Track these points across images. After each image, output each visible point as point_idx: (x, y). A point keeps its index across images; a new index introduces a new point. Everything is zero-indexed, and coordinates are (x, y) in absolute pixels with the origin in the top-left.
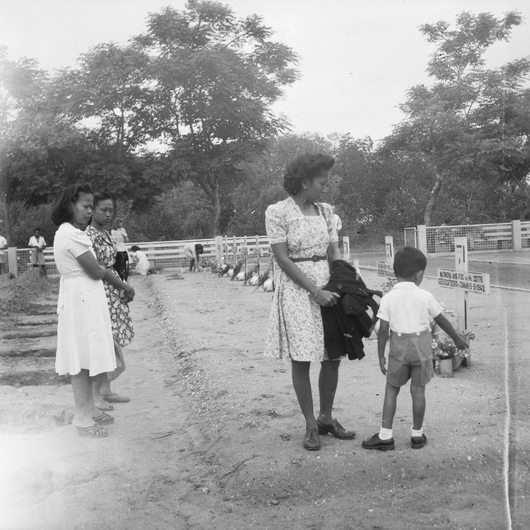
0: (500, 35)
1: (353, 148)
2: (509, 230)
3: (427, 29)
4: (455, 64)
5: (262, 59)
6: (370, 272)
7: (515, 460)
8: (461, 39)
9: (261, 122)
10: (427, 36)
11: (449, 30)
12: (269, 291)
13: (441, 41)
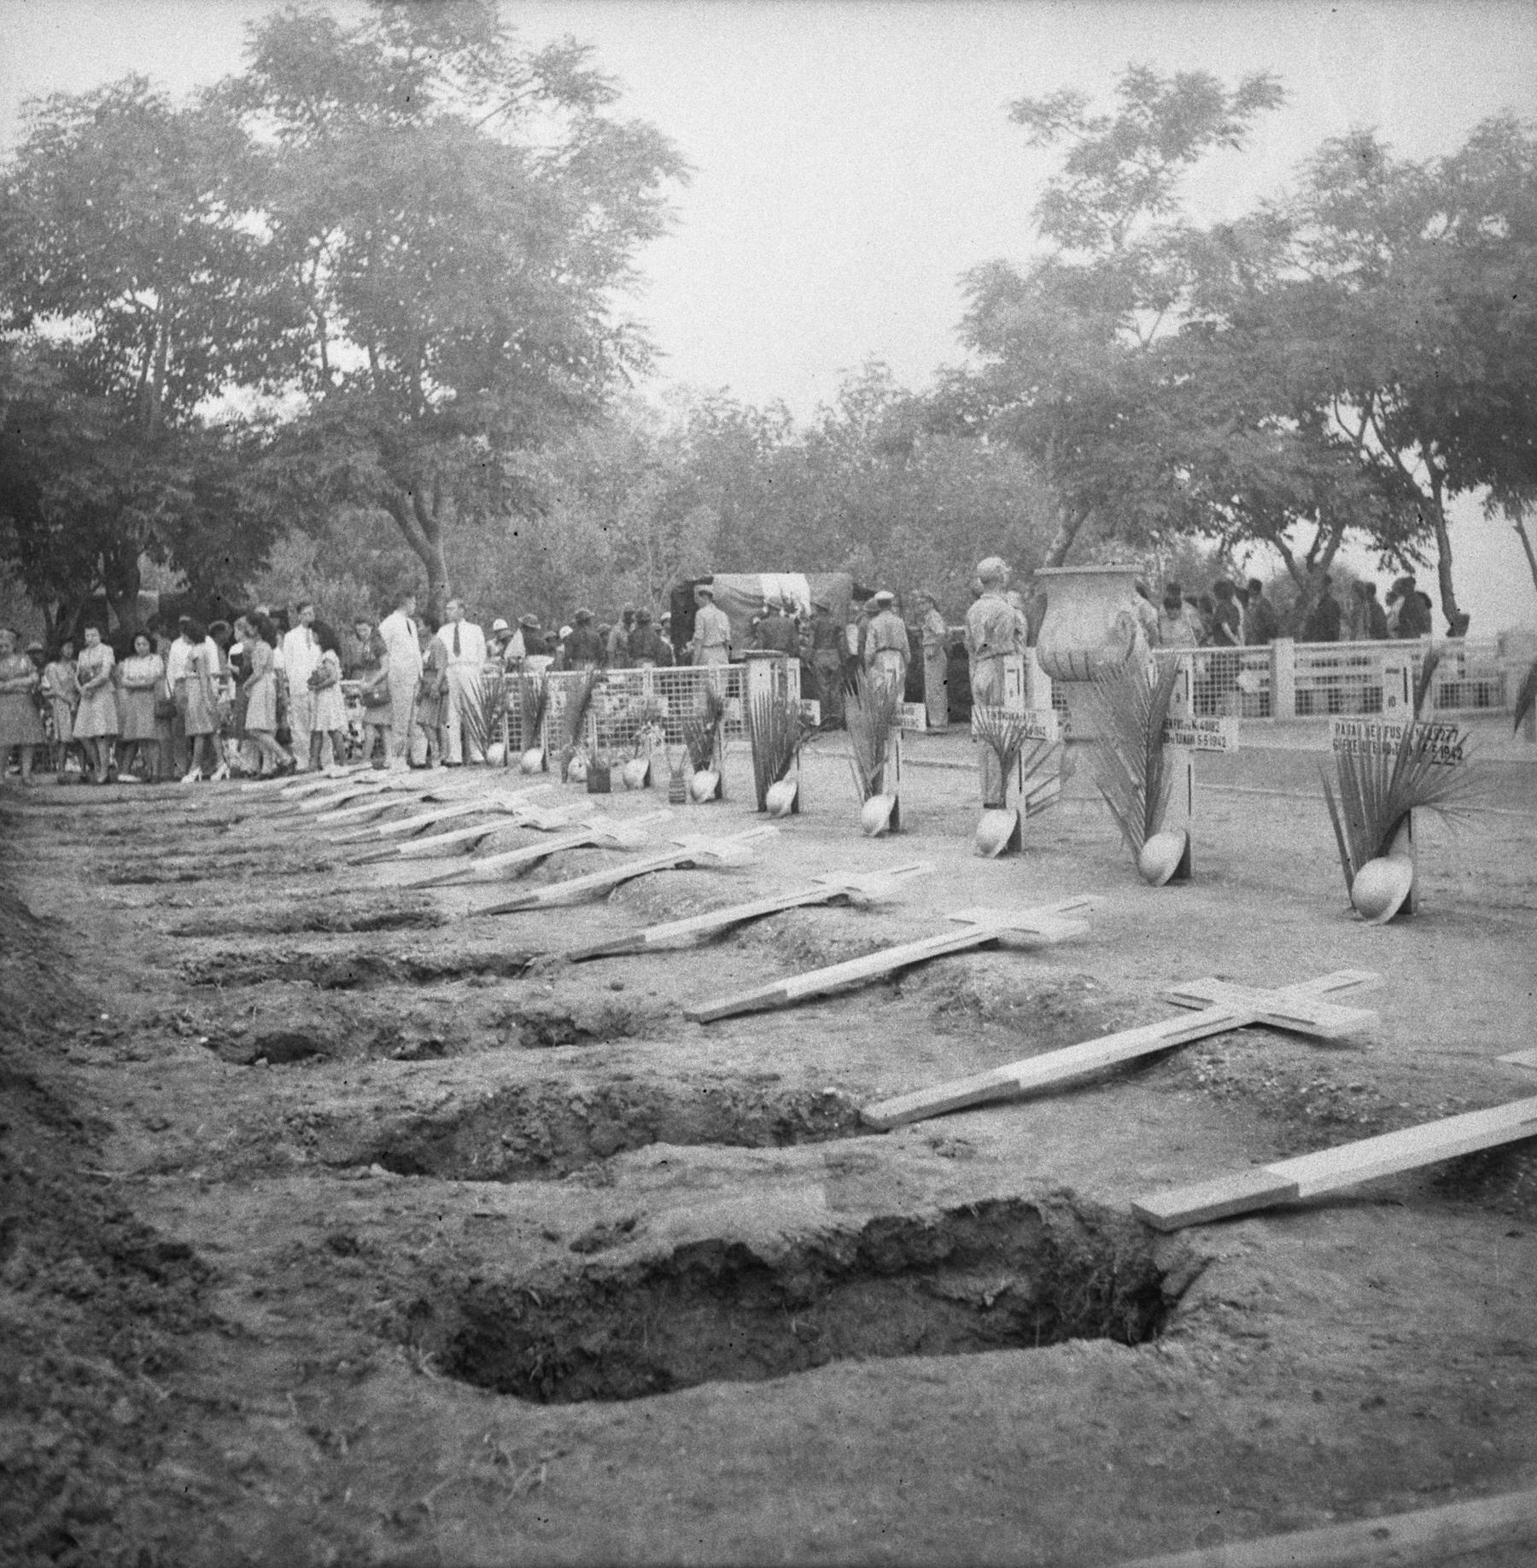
0: (1230, 136)
1: (735, 431)
2: (1265, 666)
3: (1027, 112)
4: (1109, 204)
5: (583, 166)
6: (926, 771)
7: (768, 1187)
8: (1126, 139)
9: (1095, 274)
10: (1025, 131)
11: (1089, 114)
12: (880, 835)
13: (1070, 139)
